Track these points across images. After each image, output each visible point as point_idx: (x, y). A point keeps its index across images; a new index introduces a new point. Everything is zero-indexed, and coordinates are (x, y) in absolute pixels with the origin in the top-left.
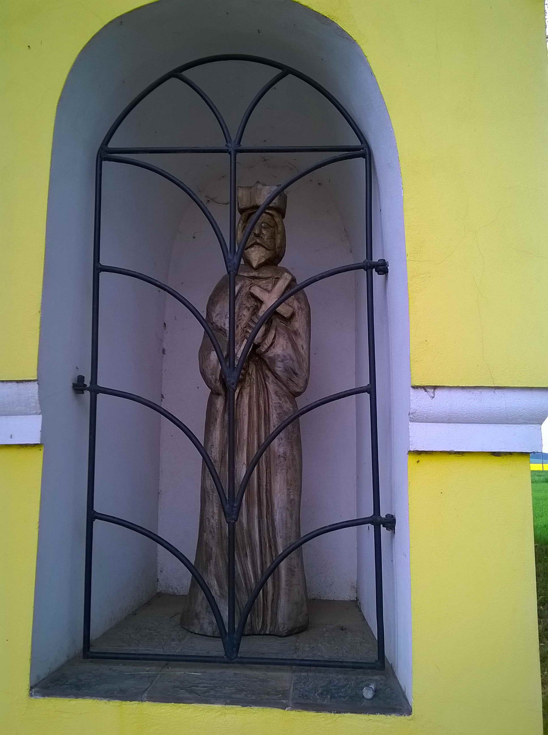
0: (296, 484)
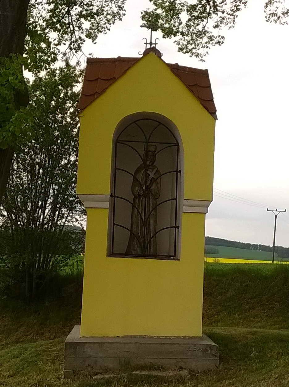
0: (155, 222)
